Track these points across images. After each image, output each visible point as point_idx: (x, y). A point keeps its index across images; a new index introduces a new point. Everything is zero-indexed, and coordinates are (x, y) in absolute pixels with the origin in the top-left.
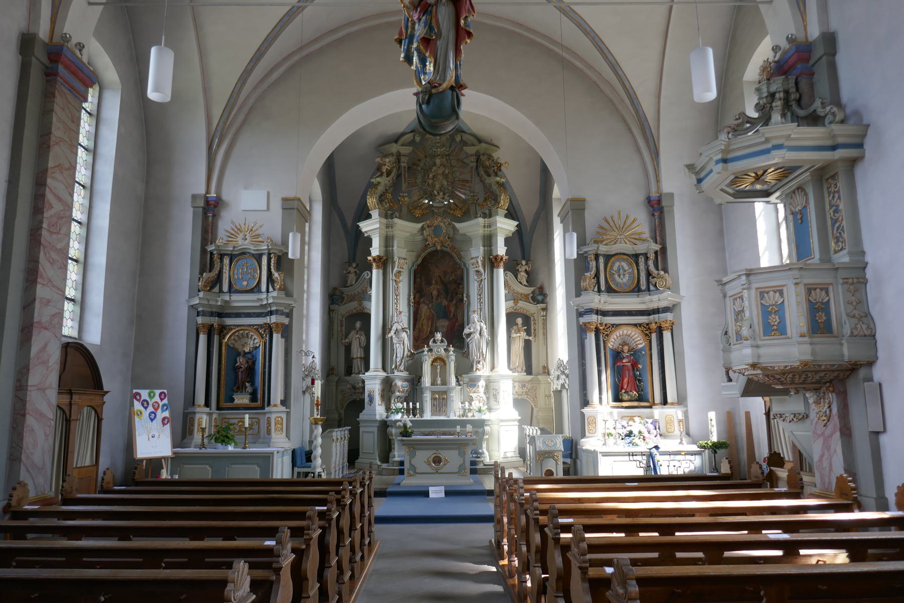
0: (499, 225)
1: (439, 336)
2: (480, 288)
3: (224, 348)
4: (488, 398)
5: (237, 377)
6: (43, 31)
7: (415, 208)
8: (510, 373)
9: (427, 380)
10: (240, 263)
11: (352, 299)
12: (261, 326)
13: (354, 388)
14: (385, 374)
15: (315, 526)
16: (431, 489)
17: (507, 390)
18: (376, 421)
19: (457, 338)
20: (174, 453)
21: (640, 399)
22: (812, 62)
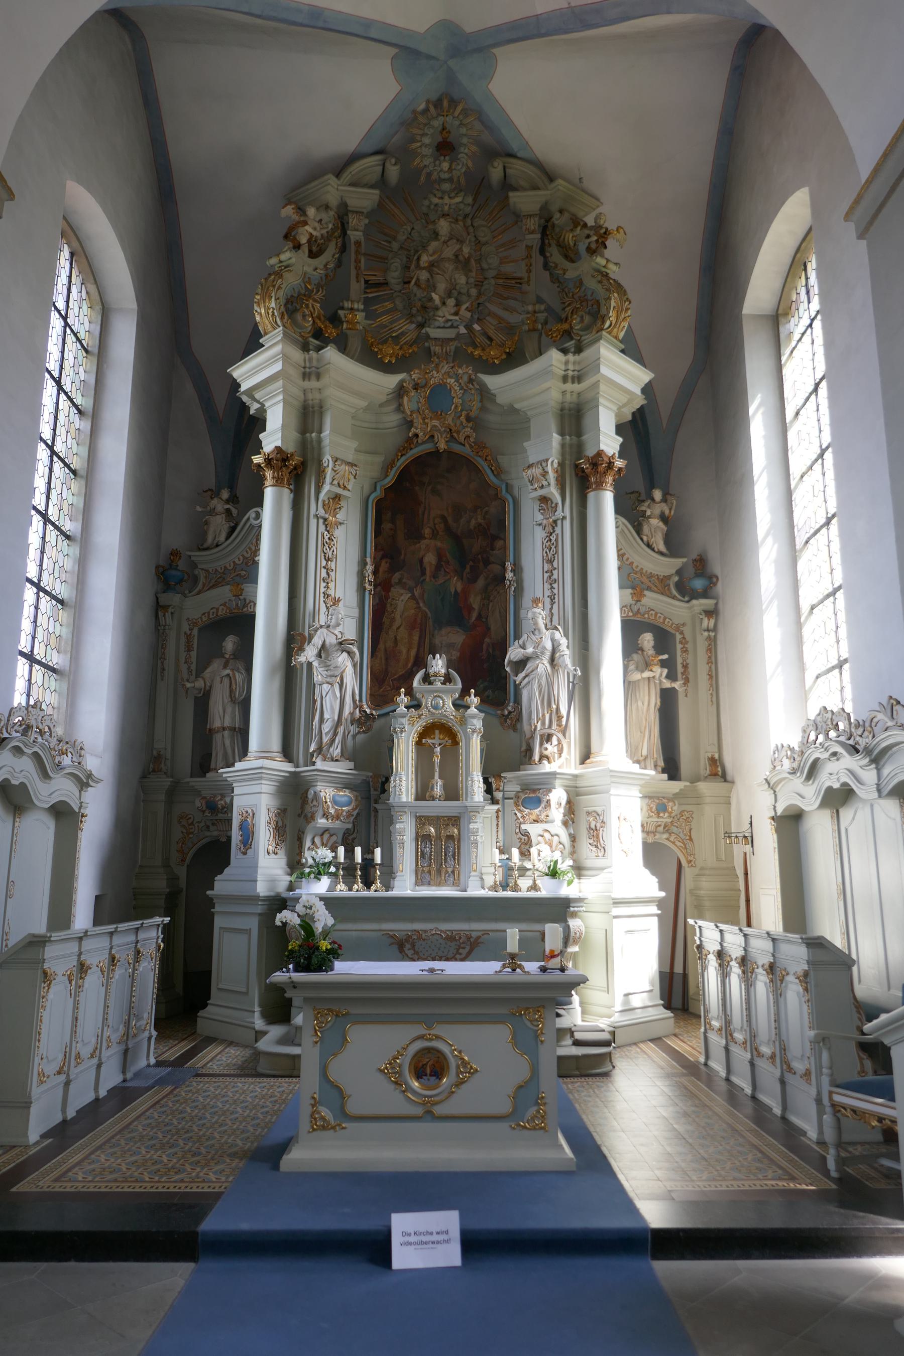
0: (604, 370)
1: (438, 665)
4: (573, 838)
7: (385, 342)
8: (636, 768)
9: (404, 786)
11: (218, 580)
14: (289, 767)
16: (402, 1224)
17: (626, 814)
18: (255, 898)
19: (489, 675)
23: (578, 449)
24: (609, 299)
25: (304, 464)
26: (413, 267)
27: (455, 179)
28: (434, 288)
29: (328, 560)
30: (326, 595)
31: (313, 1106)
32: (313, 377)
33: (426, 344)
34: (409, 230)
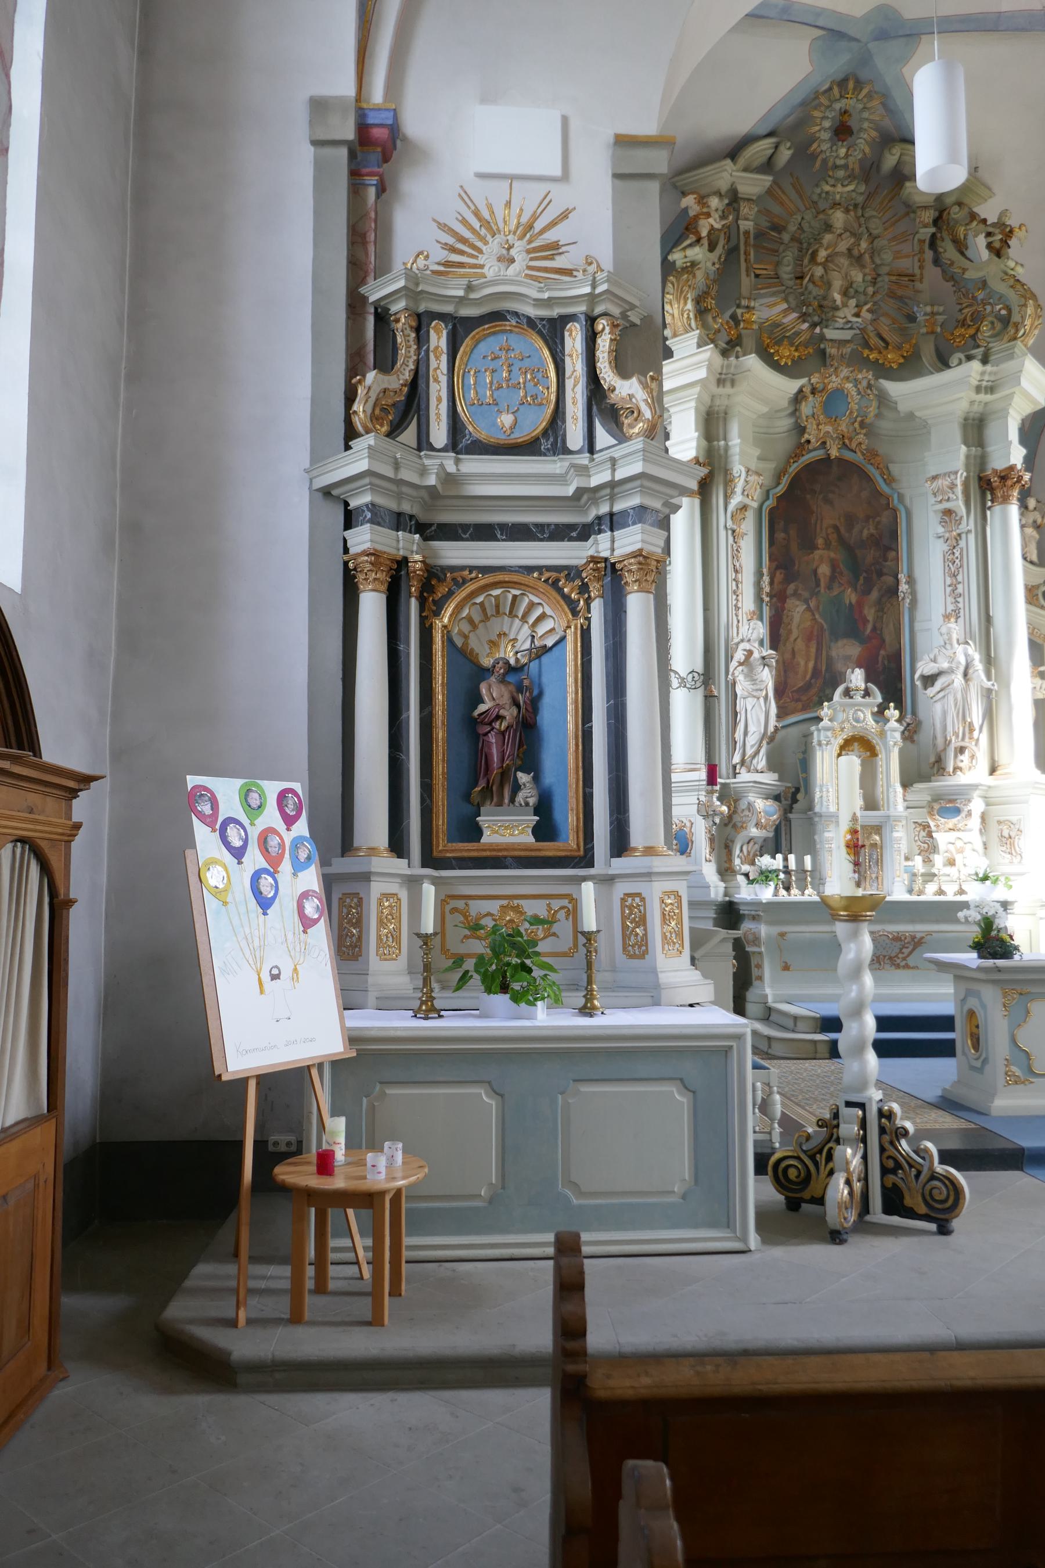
7: (779, 343)
10: (483, 348)
20: (353, 1039)
23: (982, 460)
24: (1025, 305)
26: (806, 261)
27: (851, 167)
28: (829, 285)
29: (736, 571)
30: (736, 606)
31: (1007, 1066)
32: (728, 384)
33: (822, 346)
34: (800, 219)
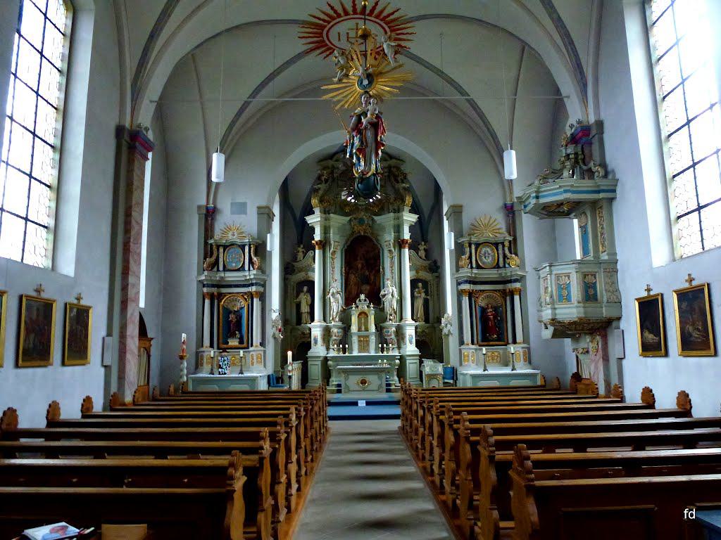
1: (362, 297)
2: (392, 263)
3: (221, 308)
5: (229, 327)
6: (127, 125)
8: (414, 322)
9: (354, 328)
12: (245, 293)
13: (303, 333)
14: (325, 324)
15: (282, 431)
18: (320, 357)
19: (375, 298)
21: (499, 339)
22: (591, 137)
25: (326, 243)
